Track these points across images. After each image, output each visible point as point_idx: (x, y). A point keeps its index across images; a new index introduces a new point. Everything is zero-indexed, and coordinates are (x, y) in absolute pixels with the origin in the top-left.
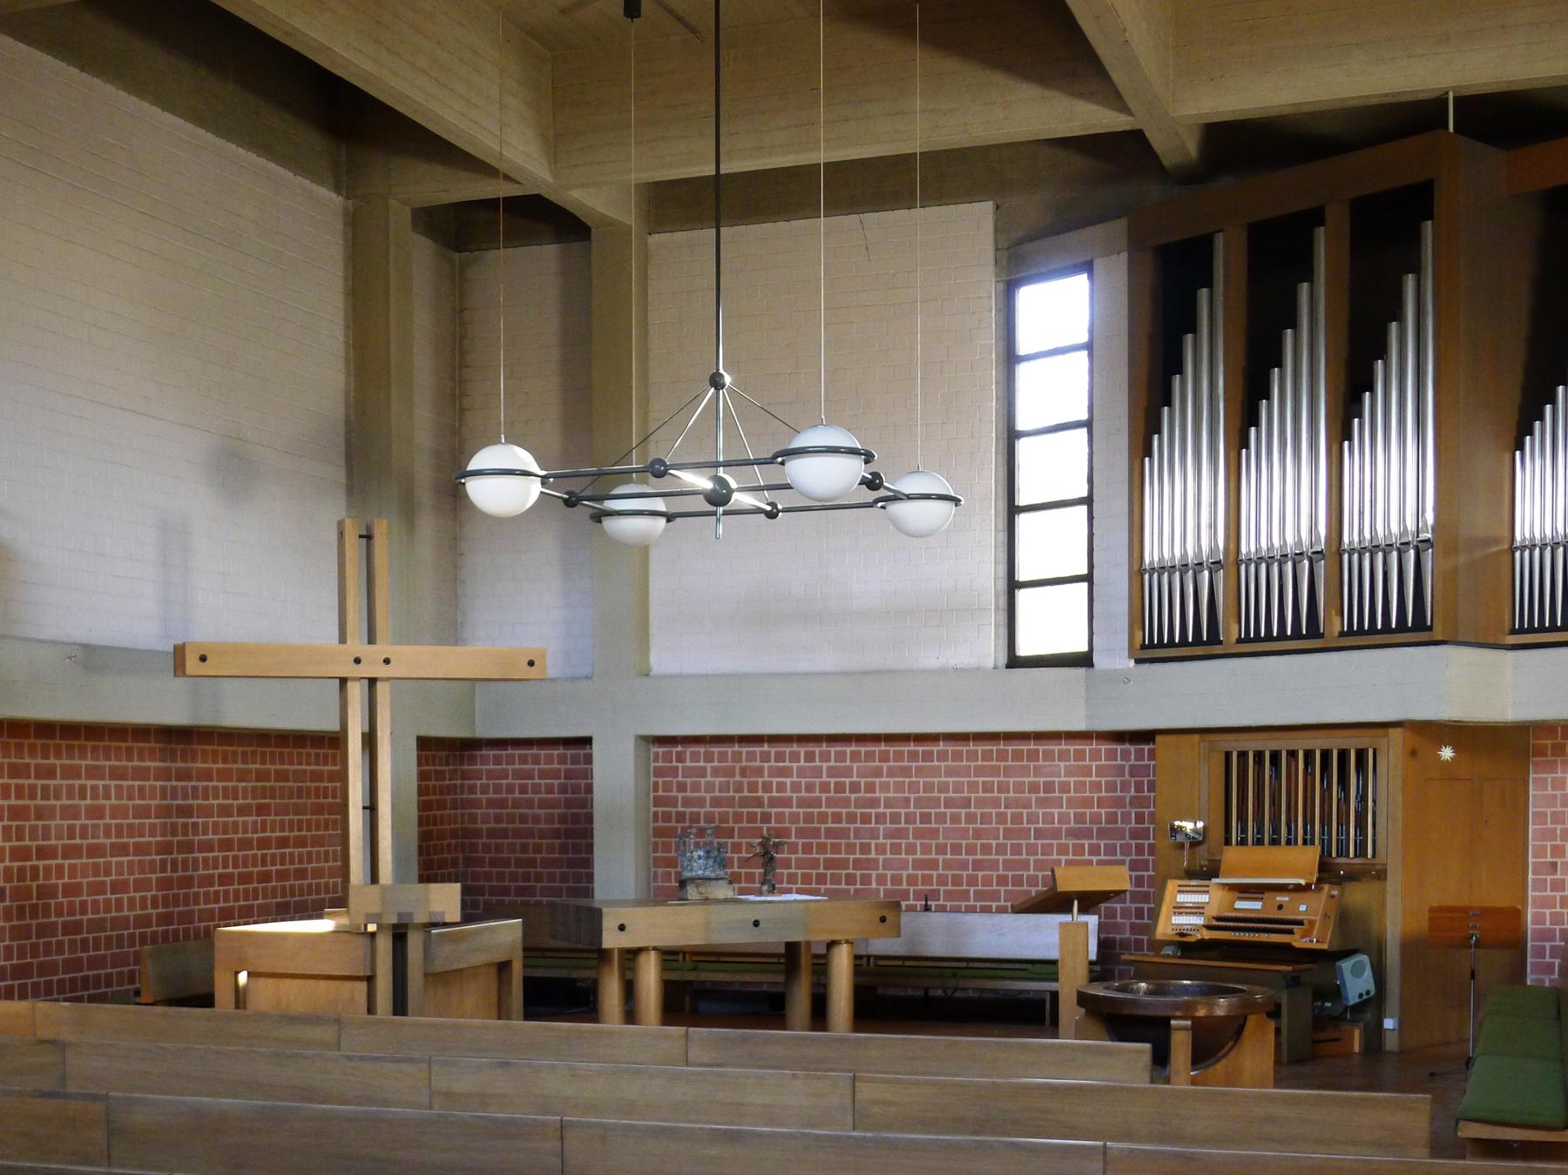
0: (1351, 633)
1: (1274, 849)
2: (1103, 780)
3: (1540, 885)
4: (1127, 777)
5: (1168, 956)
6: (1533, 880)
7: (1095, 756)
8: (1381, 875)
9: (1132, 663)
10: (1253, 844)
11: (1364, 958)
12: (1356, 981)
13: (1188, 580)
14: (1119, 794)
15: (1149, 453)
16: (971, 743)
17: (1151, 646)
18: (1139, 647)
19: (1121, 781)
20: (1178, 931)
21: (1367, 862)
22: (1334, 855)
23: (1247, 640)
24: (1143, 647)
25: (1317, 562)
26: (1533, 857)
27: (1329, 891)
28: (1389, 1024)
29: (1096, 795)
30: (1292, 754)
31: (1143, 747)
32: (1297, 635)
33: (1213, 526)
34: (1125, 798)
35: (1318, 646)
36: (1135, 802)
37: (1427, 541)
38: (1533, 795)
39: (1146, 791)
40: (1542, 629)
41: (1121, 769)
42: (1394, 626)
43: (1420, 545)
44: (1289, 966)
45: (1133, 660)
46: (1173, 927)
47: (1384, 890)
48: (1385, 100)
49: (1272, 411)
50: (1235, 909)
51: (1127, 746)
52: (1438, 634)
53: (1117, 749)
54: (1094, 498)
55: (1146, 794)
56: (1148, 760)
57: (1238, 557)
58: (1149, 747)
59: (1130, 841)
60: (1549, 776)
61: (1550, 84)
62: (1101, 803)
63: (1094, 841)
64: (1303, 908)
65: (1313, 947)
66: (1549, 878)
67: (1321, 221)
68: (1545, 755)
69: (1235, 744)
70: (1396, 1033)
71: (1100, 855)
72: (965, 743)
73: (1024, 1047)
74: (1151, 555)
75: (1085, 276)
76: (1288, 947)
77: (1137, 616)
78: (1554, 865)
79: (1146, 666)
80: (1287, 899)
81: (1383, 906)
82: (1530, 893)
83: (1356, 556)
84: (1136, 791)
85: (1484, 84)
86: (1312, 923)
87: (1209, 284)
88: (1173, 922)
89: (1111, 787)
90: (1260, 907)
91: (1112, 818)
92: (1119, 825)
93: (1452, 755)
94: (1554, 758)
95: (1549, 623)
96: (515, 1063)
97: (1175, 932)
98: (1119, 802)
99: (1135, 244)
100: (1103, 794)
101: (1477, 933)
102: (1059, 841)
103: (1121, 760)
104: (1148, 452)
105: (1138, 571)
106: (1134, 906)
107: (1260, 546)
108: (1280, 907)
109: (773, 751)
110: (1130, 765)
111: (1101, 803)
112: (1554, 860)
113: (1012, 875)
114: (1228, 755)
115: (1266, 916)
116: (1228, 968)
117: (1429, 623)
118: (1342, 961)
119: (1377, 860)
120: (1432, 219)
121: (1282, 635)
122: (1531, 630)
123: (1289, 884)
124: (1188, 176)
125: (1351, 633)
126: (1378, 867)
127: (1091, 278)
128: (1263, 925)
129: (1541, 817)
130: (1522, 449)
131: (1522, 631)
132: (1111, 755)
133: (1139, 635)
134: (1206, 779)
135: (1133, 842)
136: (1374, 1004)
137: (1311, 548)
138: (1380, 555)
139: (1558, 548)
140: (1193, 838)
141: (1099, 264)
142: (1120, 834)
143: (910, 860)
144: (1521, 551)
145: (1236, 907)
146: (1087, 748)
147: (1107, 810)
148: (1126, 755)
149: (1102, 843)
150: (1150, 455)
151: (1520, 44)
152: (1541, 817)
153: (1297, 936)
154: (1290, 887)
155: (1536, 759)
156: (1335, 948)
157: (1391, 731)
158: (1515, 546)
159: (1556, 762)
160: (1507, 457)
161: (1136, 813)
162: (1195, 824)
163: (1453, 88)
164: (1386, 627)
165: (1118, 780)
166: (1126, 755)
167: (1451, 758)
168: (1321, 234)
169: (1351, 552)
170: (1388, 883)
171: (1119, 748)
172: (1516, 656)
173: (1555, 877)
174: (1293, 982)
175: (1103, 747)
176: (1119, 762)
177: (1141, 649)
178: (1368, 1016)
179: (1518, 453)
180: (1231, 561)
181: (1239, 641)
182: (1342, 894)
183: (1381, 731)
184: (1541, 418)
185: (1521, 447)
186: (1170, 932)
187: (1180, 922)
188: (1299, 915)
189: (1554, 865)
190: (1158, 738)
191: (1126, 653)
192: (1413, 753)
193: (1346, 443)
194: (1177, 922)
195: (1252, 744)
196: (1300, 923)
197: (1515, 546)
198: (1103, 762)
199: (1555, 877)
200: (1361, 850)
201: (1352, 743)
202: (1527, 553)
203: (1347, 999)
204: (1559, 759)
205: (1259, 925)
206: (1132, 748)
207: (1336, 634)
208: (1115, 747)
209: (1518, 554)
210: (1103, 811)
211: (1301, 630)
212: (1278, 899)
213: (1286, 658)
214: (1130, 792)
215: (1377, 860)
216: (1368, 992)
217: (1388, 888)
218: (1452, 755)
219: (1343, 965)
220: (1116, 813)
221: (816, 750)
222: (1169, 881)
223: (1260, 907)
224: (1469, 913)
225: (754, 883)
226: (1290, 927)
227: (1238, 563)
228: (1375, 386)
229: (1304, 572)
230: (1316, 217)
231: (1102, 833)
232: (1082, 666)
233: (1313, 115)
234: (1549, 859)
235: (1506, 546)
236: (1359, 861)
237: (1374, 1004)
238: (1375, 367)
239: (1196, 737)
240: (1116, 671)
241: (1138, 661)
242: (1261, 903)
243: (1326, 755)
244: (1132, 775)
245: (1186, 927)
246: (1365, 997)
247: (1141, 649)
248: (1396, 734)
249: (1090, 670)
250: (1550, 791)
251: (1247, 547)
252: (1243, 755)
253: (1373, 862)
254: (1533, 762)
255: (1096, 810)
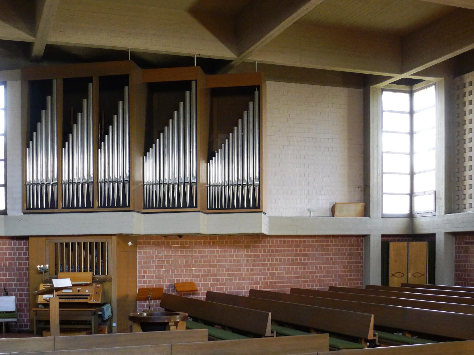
0: (101, 207)
2: (7, 252)
3: (140, 282)
4: (15, 251)
5: (42, 308)
6: (138, 280)
8: (110, 280)
11: (109, 305)
12: (107, 312)
13: (44, 188)
14: (13, 256)
15: (28, 146)
16: (4, 240)
17: (30, 208)
19: (13, 252)
21: (106, 276)
22: (94, 274)
24: (27, 209)
26: (138, 274)
27: (96, 285)
28: (114, 325)
29: (5, 257)
30: (79, 244)
34: (15, 258)
35: (128, 210)
39: (23, 255)
40: (153, 208)
42: (116, 206)
44: (94, 308)
45: (22, 213)
46: (44, 299)
47: (111, 284)
48: (112, 48)
49: (74, 137)
51: (15, 241)
52: (131, 208)
53: (12, 242)
54: (7, 159)
58: (23, 241)
60: (142, 251)
61: (65, 44)
64: (87, 291)
65: (94, 303)
66: (143, 280)
67: (92, 81)
69: (59, 241)
71: (7, 277)
73: (24, 341)
74: (29, 179)
75: (3, 86)
76: (86, 303)
77: (25, 199)
78: (144, 276)
80: (81, 288)
81: (111, 290)
86: (92, 295)
87: (51, 94)
89: (10, 254)
91: (10, 264)
92: (13, 267)
94: (143, 245)
96: (46, 352)
98: (13, 259)
99: (24, 78)
101: (151, 296)
105: (25, 185)
107: (150, 181)
108: (79, 291)
109: (166, 241)
110: (16, 247)
112: (144, 275)
113: (9, 284)
116: (62, 310)
117: (92, 206)
118: (104, 306)
119: (109, 276)
122: (149, 208)
123: (83, 284)
124: (38, 60)
125: (101, 207)
126: (109, 278)
127: (5, 87)
129: (140, 262)
130: (146, 156)
131: (146, 208)
132: (10, 244)
133: (25, 205)
134: (49, 252)
139: (150, 185)
140: (40, 271)
141: (8, 83)
144: (146, 185)
145: (63, 291)
149: (7, 273)
150: (29, 147)
151: (150, 40)
152: (140, 262)
153: (89, 300)
154: (83, 285)
155: (138, 246)
157: (113, 237)
158: (144, 184)
159: (144, 246)
161: (19, 263)
162: (40, 266)
163: (131, 49)
165: (12, 252)
166: (15, 244)
167: (131, 245)
168: (91, 85)
170: (113, 282)
171: (13, 241)
172: (145, 216)
173: (144, 280)
174: (94, 313)
178: (109, 323)
179: (145, 157)
180: (59, 183)
181: (99, 207)
182: (103, 286)
183: (109, 237)
184: (152, 148)
186: (42, 300)
187: (46, 297)
189: (144, 276)
190: (30, 239)
192: (118, 243)
194: (44, 297)
196: (89, 296)
197: (144, 184)
198: (7, 246)
199: (144, 280)
200: (104, 273)
201: (100, 240)
202: (148, 186)
204: (145, 246)
206: (17, 242)
207: (61, 208)
208: (11, 241)
209: (145, 186)
211: (110, 205)
212: (78, 288)
213: (151, 215)
214: (16, 256)
215: (109, 276)
216: (110, 316)
219: (104, 308)
221: (345, 239)
224: (149, 290)
225: (2, 287)
227: (62, 184)
228: (109, 133)
230: (90, 79)
231: (7, 270)
232: (3, 215)
233: (144, 53)
234: (143, 275)
236: (103, 276)
238: (109, 128)
239: (44, 238)
241: (24, 213)
242: (72, 290)
243: (84, 244)
244: (17, 250)
245: (47, 299)
246: (109, 317)
248: (114, 238)
249: (6, 216)
250: (143, 255)
251: (65, 178)
252: (67, 245)
253: (107, 276)
255: (5, 262)
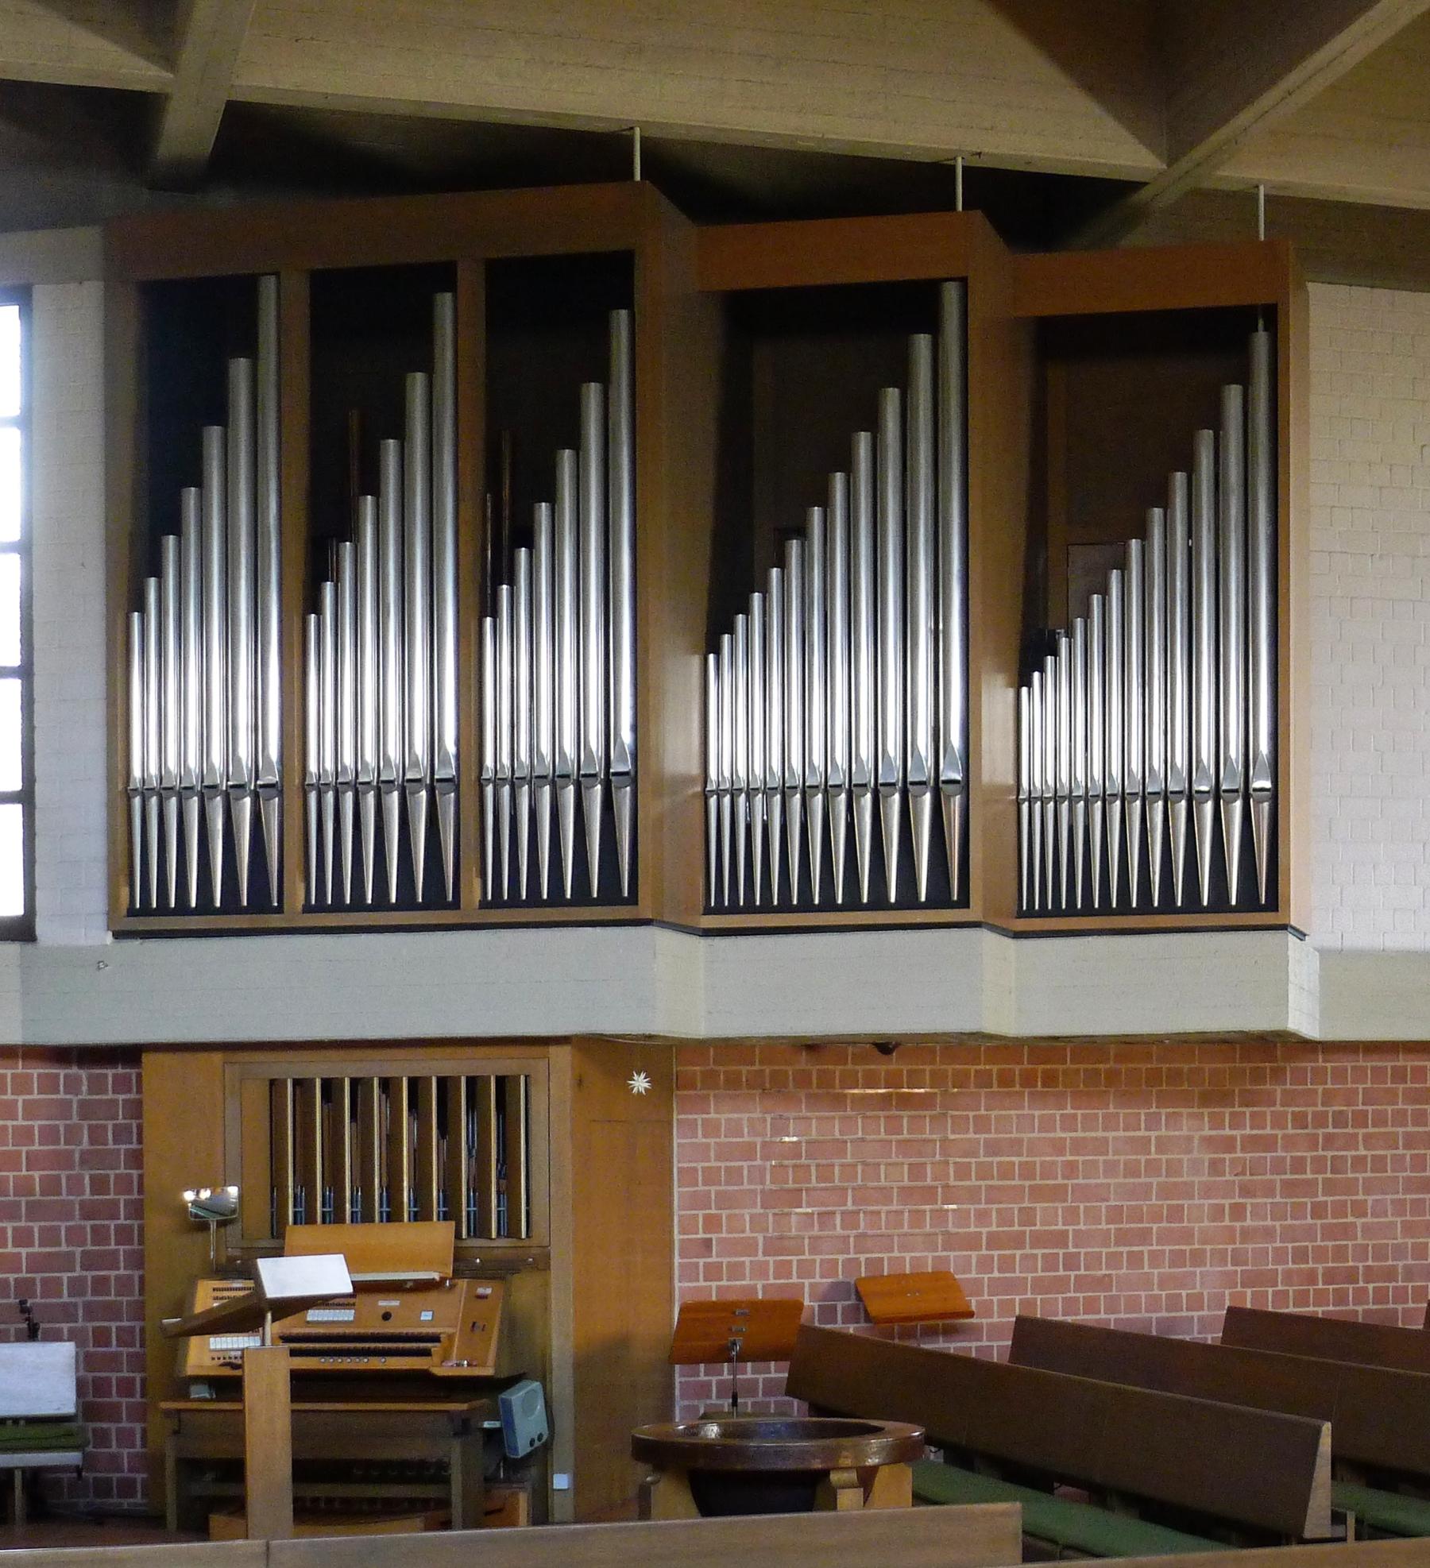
1: (362, 1228)
2: (37, 1124)
3: (690, 1272)
4: (75, 1119)
7: (22, 1085)
8: (542, 1264)
9: (109, 938)
10: (410, 1220)
14: (62, 1146)
15: (140, 606)
17: (146, 911)
18: (124, 912)
19: (67, 1127)
20: (222, 1361)
23: (321, 907)
24: (132, 912)
25: (619, 788)
28: (561, 1481)
29: (24, 1149)
31: (104, 1071)
32: (406, 901)
33: (258, 728)
36: (86, 1160)
37: (272, 786)
38: (679, 1145)
40: (749, 908)
41: (64, 1109)
43: (230, 791)
46: (215, 1355)
48: (551, 123)
50: (308, 1322)
51: (74, 1070)
52: (644, 910)
54: (36, 669)
55: (111, 1146)
56: (114, 1092)
57: (304, 779)
58: (114, 1071)
59: (83, 1223)
60: (699, 1117)
62: (33, 1162)
63: (23, 1224)
64: (426, 1316)
66: (701, 1261)
68: (693, 1087)
69: (289, 1068)
70: (571, 1494)
72: (10, 1062)
74: (143, 765)
75: (15, 309)
76: (425, 1376)
78: (707, 1243)
79: (135, 944)
80: (395, 1303)
82: (677, 1284)
83: (506, 790)
84: (92, 1142)
85: (771, 135)
86: (451, 1337)
87: (250, 349)
88: (212, 1347)
89: (49, 1135)
90: (352, 1318)
91: (51, 1186)
92: (64, 1197)
93: (647, 1085)
95: (798, 900)
97: (216, 1362)
98: (63, 1160)
100: (36, 1147)
102: (1032, 1183)
103: (66, 1093)
104: (314, 605)
106: (90, 1325)
108: (386, 1316)
111: (33, 1162)
112: (708, 1236)
114: (275, 1085)
115: (362, 1331)
117: (450, 898)
119: (534, 1242)
120: (629, 305)
121: (182, 908)
123: (405, 1281)
126: (534, 1251)
127: (26, 313)
128: (311, 1345)
129: (689, 1175)
133: (125, 892)
135: (89, 1224)
136: (543, 1453)
137: (257, 778)
138: (174, 801)
141: (39, 292)
142: (65, 1212)
143: (24, 1256)
145: (309, 1319)
146: (9, 1072)
147: (42, 1173)
148: (97, 1086)
149: (36, 1227)
150: (142, 608)
152: (689, 1175)
153: (436, 1359)
154: (409, 1285)
155: (678, 1092)
156: (504, 1374)
157: (553, 1050)
160: (696, 661)
161: (91, 1177)
162: (198, 1193)
163: (644, 125)
164: (206, 904)
165: (61, 1124)
166: (72, 1085)
167: (646, 1089)
168: (445, 303)
169: (145, 793)
173: (709, 1260)
174: (463, 1427)
175: (35, 1072)
176: (61, 1096)
177: (304, 911)
178: (534, 1472)
179: (711, 657)
182: (507, 1294)
183: (536, 1050)
184: (747, 611)
185: (717, 651)
186: (207, 1362)
188: (419, 1327)
189: (707, 1243)
190: (147, 1058)
191: (101, 920)
192: (580, 1082)
193: (488, 621)
195: (317, 1069)
196: (435, 1339)
198: (35, 1096)
200: (510, 1229)
201: (491, 1066)
203: (516, 1449)
204: (712, 1093)
205: (367, 1345)
206: (83, 1073)
209: (713, 801)
210: (37, 1175)
214: (80, 1143)
215: (534, 1242)
216: (540, 1437)
217: (553, 1280)
218: (647, 1085)
219: (513, 1398)
220: (58, 1178)
222: (199, 1282)
223: (352, 1318)
224: (734, 1313)
226: (422, 1345)
229: (420, 811)
230: (444, 276)
231: (35, 1211)
234: (701, 1235)
235: (699, 789)
237: (543, 1453)
239: (217, 1057)
240: (79, 949)
241: (119, 935)
245: (233, 1354)
246: (537, 1444)
247: (304, 911)
248: (561, 1056)
249: (29, 947)
250: (700, 1139)
252: (330, 1088)
253: (527, 1243)
254: (676, 1095)
